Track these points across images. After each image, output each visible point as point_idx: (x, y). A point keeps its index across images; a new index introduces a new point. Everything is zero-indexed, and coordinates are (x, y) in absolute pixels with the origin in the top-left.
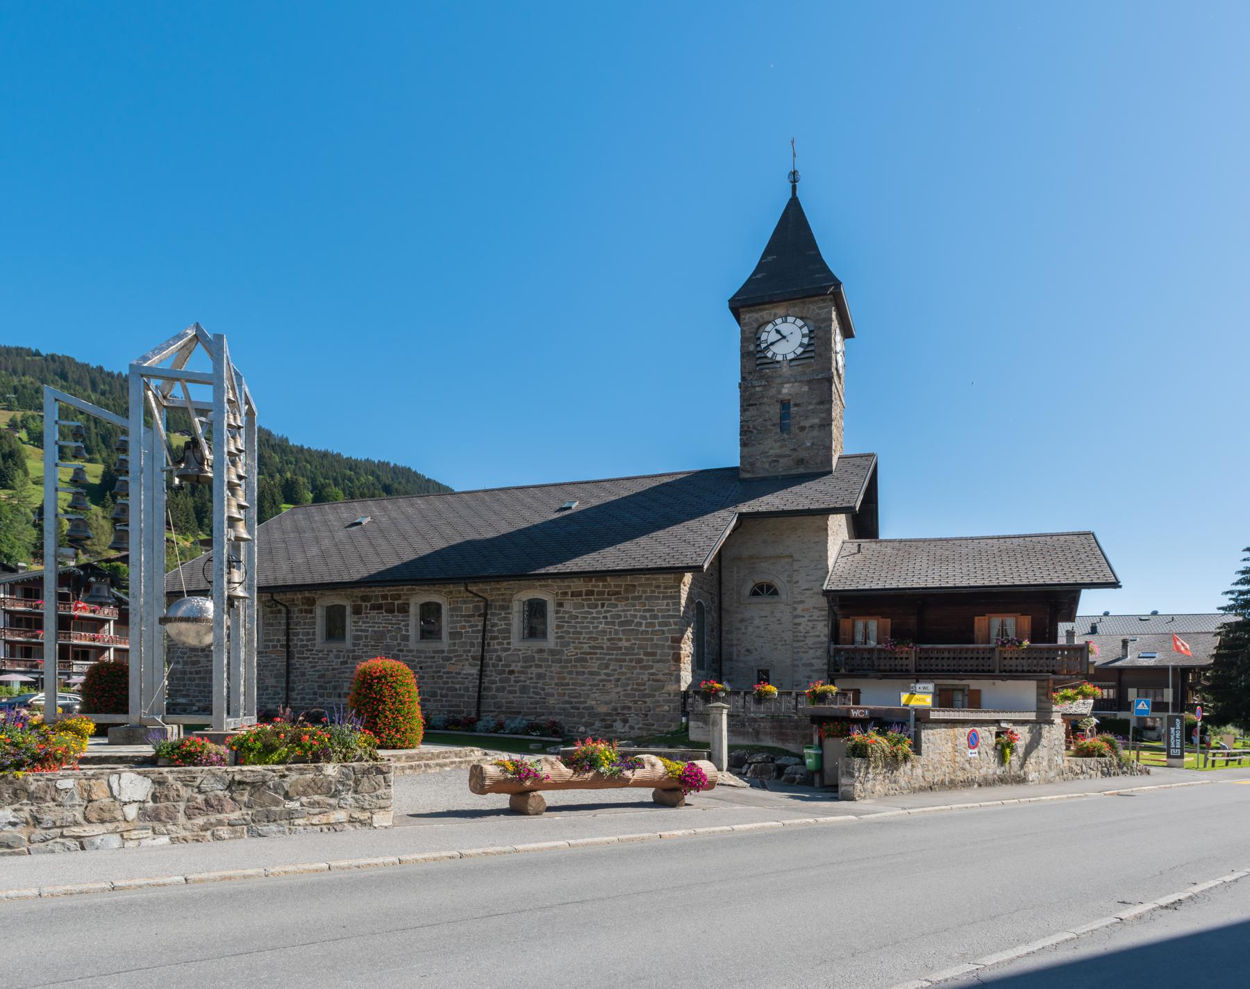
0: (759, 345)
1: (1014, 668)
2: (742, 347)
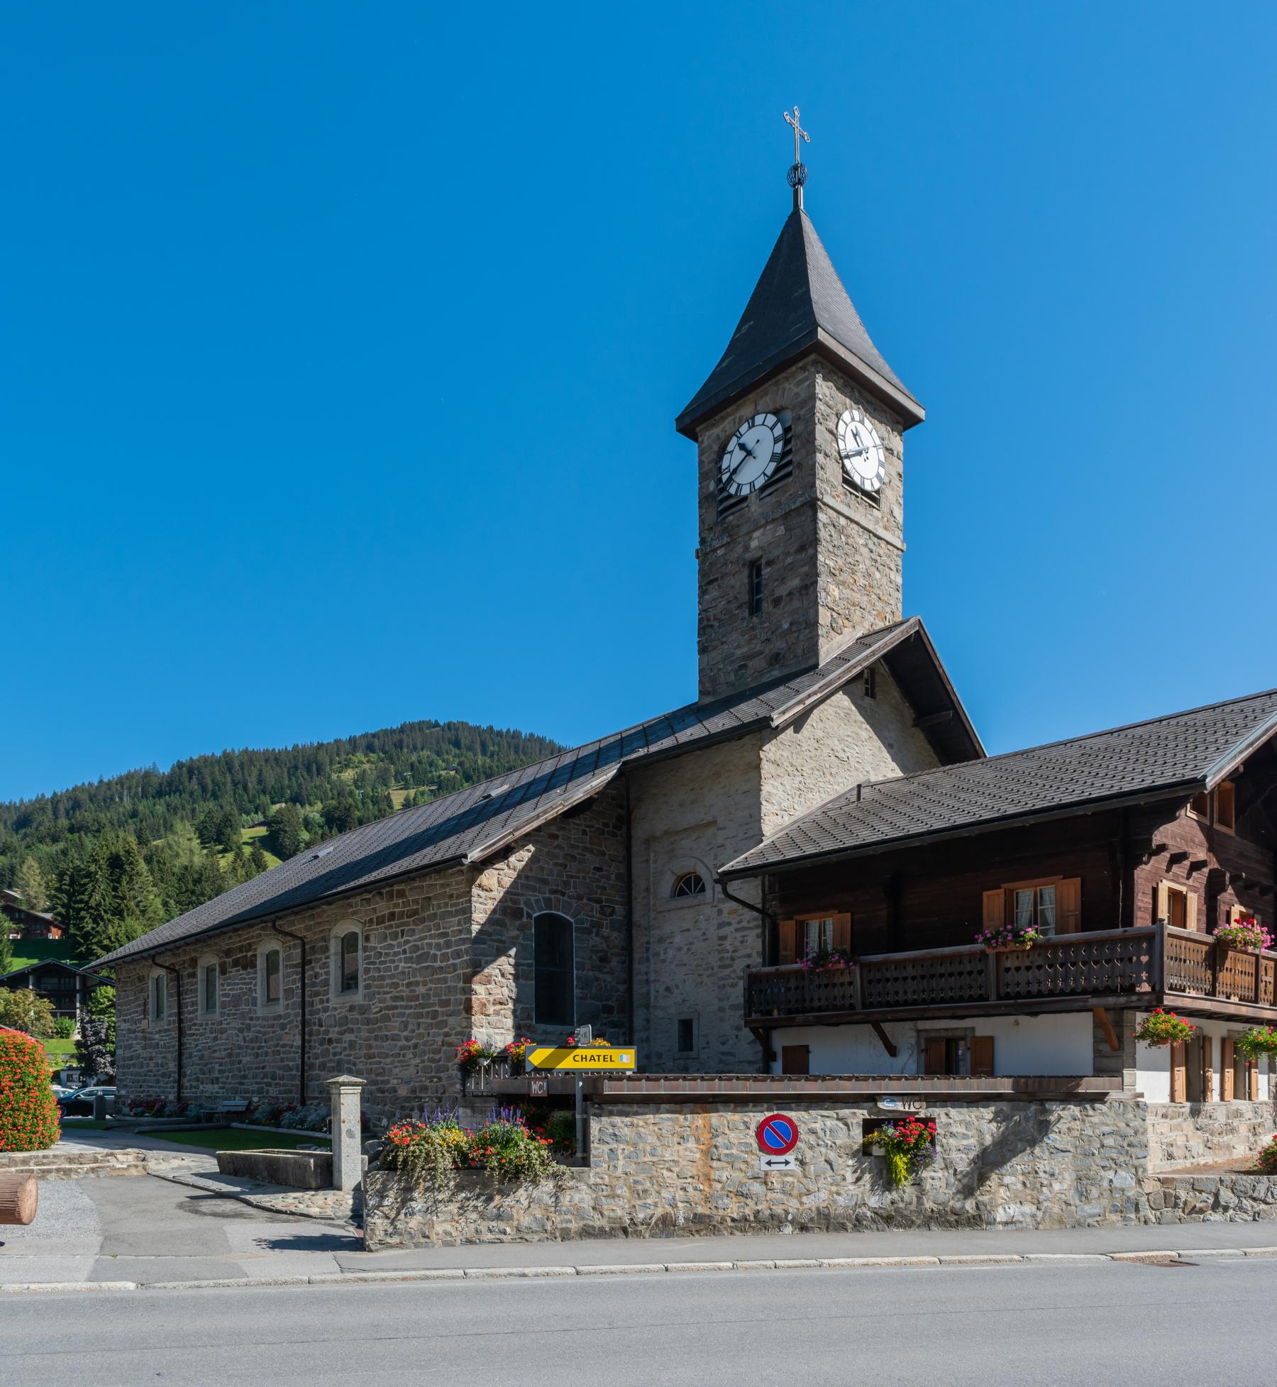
1: (1022, 989)
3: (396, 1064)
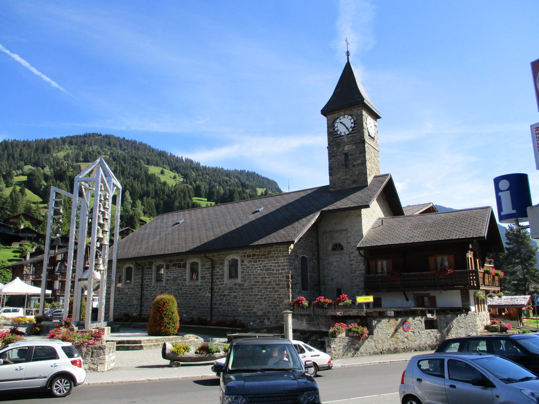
0: (334, 129)
2: (328, 130)
3: (256, 304)
